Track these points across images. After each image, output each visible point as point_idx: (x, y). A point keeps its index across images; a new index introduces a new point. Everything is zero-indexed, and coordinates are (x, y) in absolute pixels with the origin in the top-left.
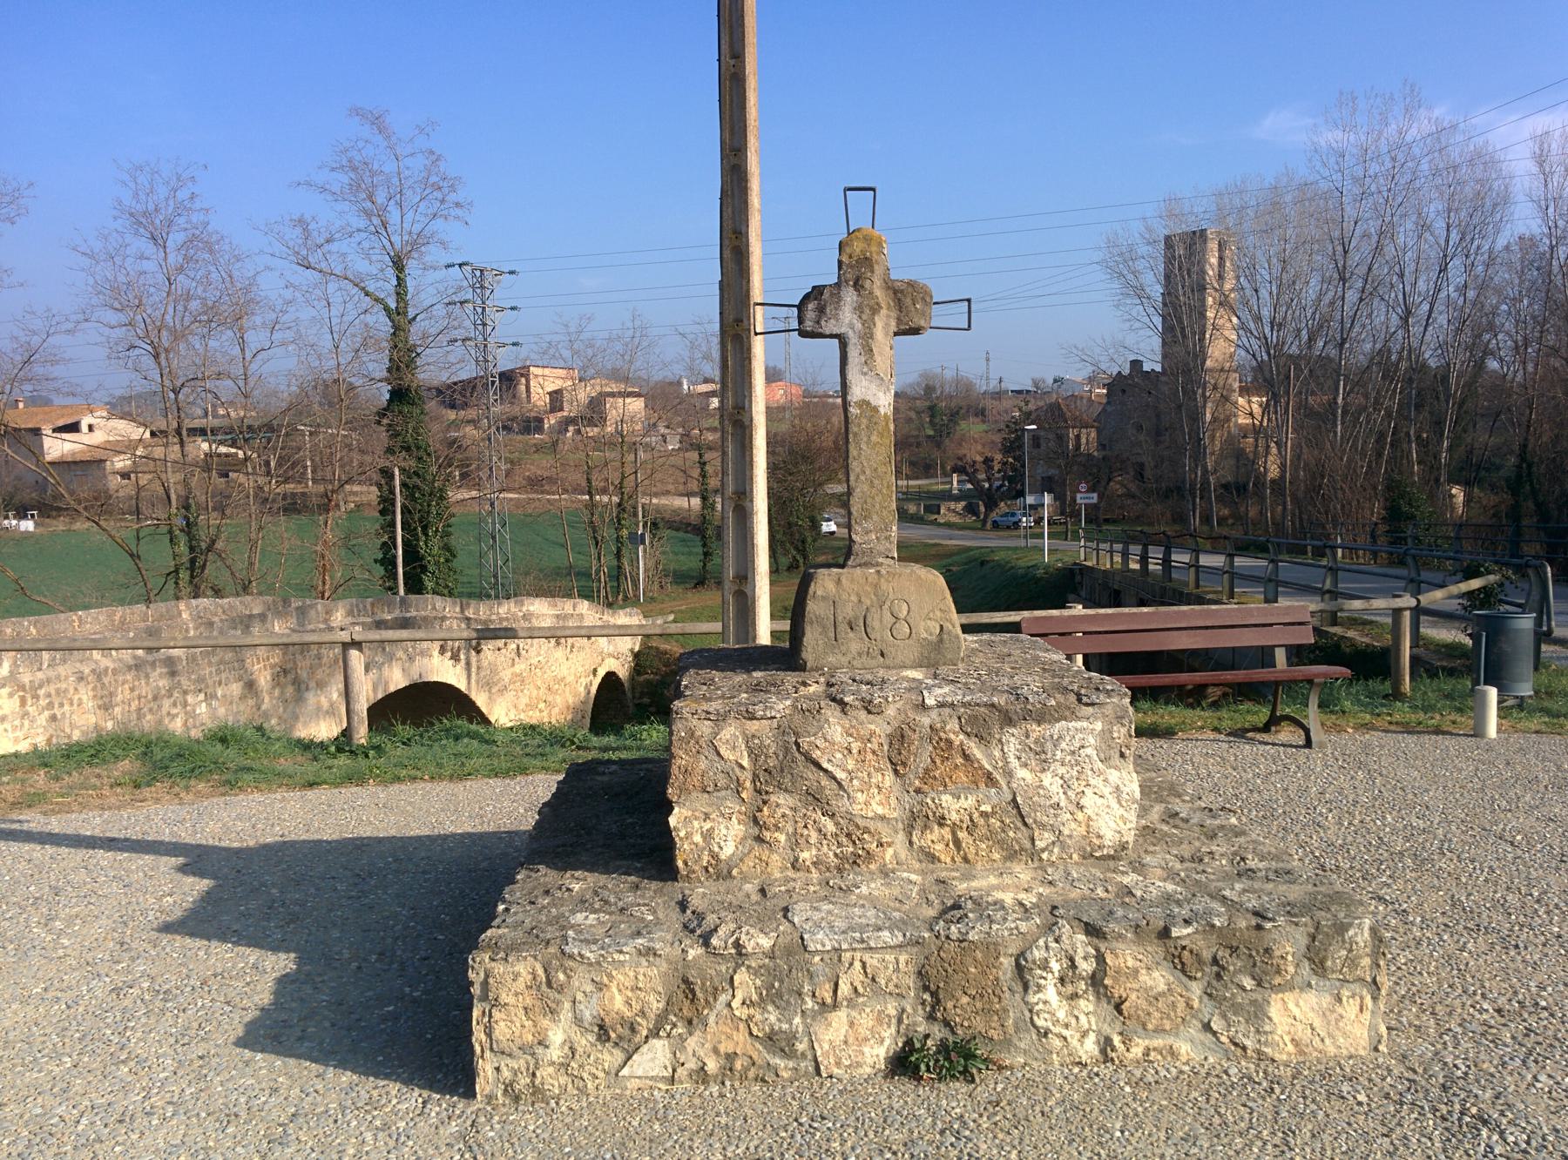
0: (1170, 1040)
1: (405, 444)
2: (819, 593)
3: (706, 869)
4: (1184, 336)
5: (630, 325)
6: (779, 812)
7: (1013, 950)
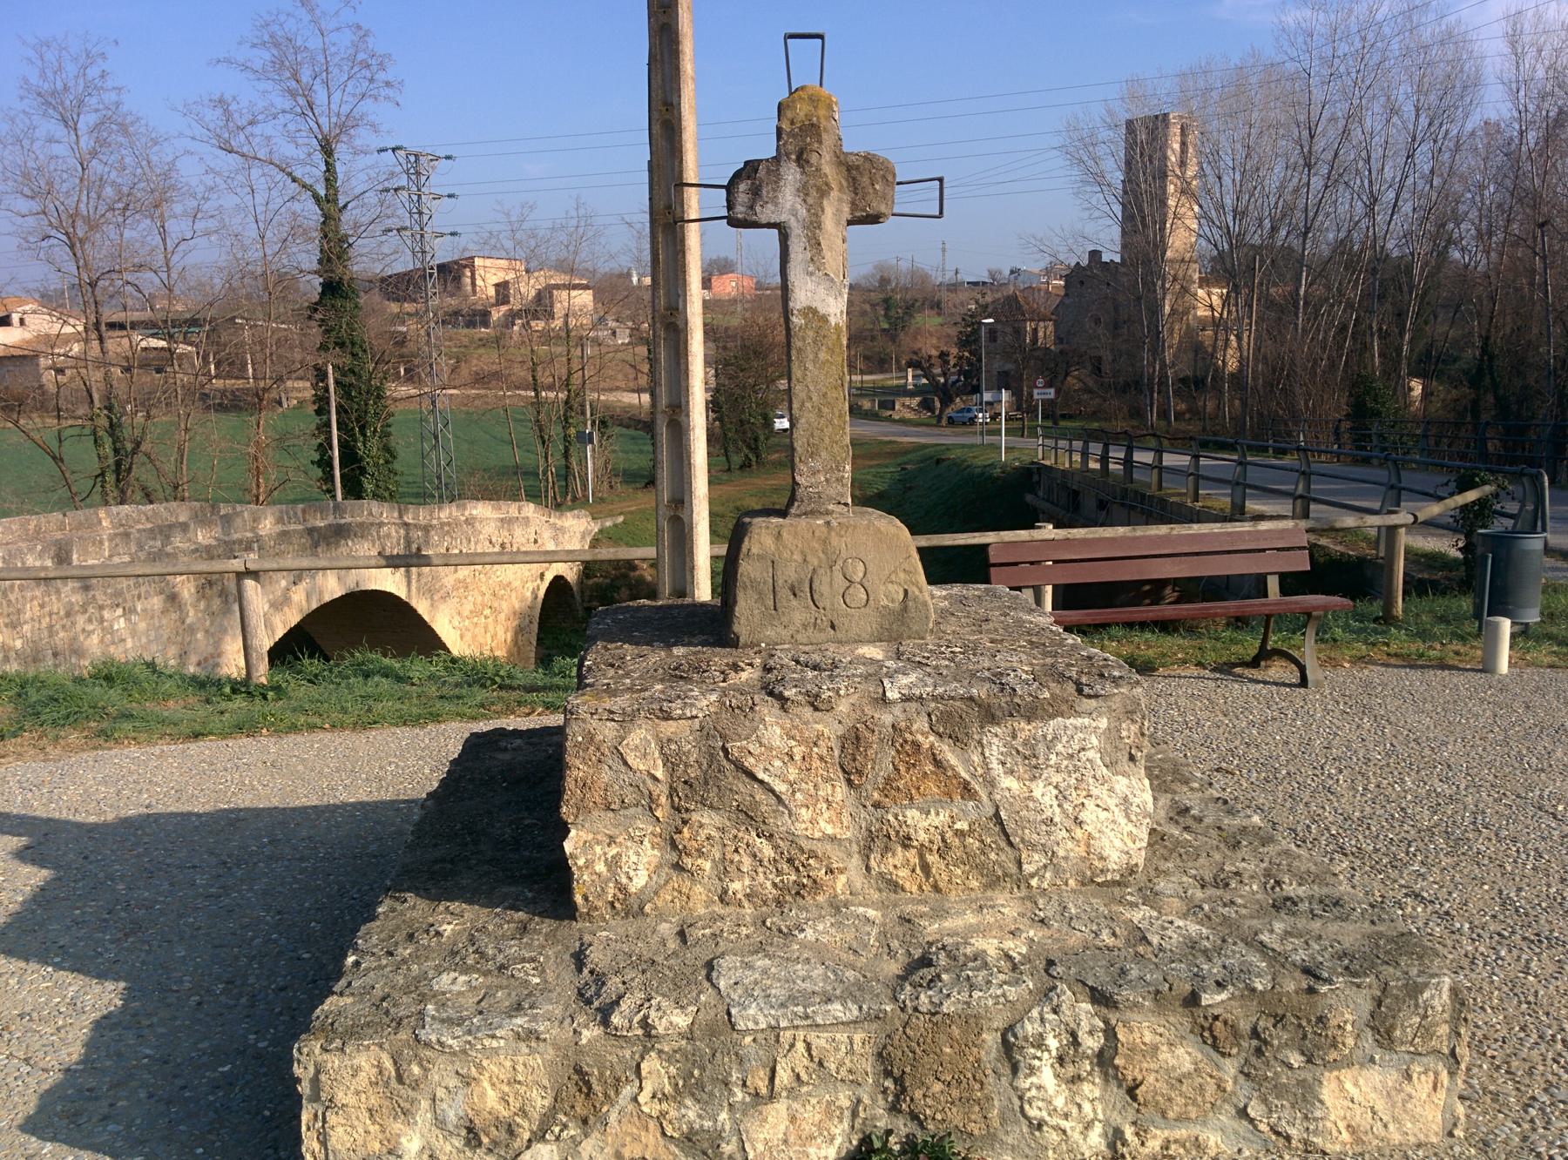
0: (1195, 1130)
1: (341, 340)
2: (754, 550)
3: (612, 904)
4: (1144, 226)
5: (574, 214)
6: (703, 834)
7: (999, 1023)
